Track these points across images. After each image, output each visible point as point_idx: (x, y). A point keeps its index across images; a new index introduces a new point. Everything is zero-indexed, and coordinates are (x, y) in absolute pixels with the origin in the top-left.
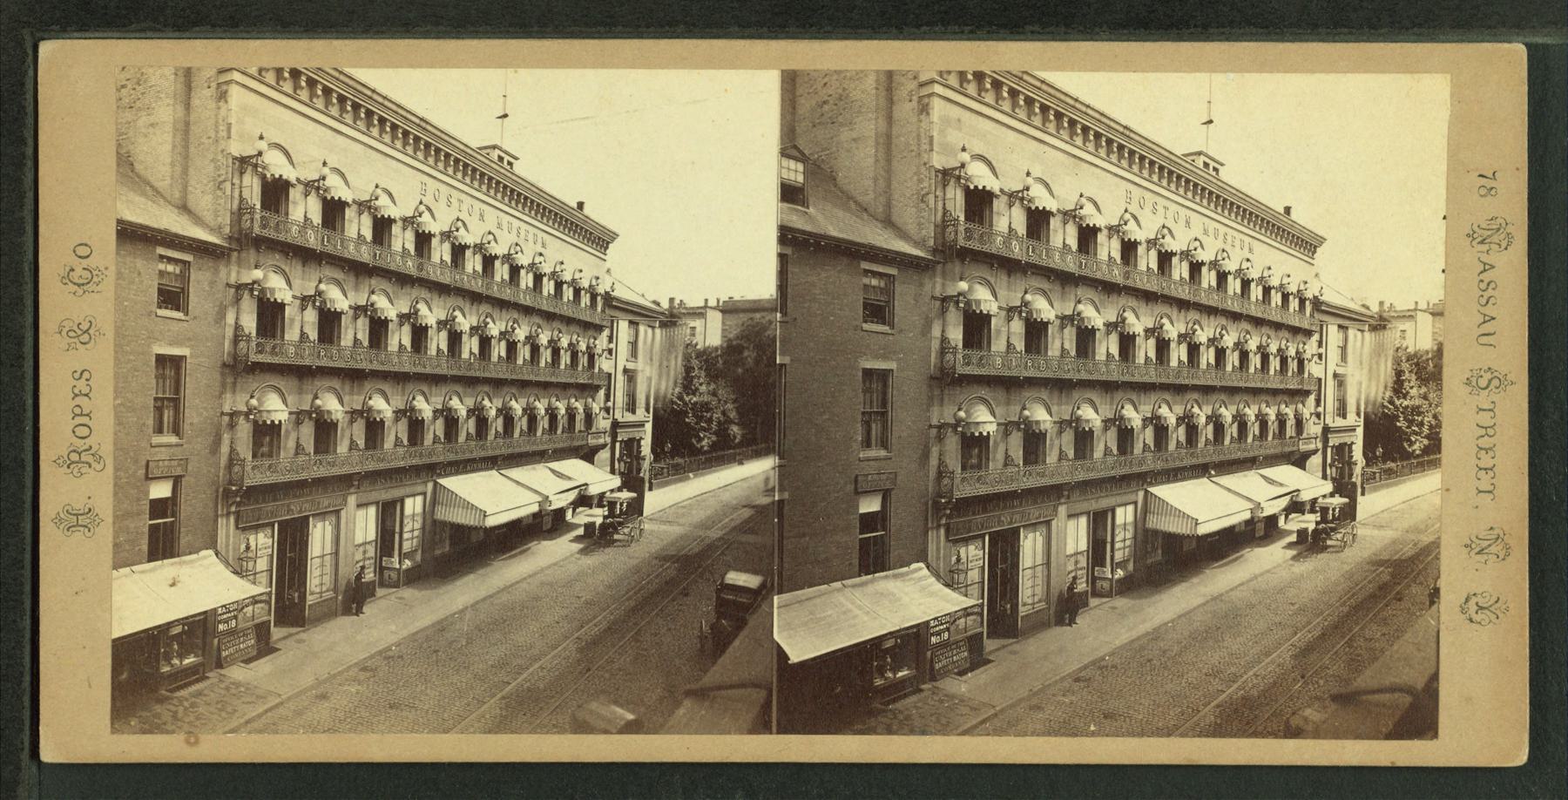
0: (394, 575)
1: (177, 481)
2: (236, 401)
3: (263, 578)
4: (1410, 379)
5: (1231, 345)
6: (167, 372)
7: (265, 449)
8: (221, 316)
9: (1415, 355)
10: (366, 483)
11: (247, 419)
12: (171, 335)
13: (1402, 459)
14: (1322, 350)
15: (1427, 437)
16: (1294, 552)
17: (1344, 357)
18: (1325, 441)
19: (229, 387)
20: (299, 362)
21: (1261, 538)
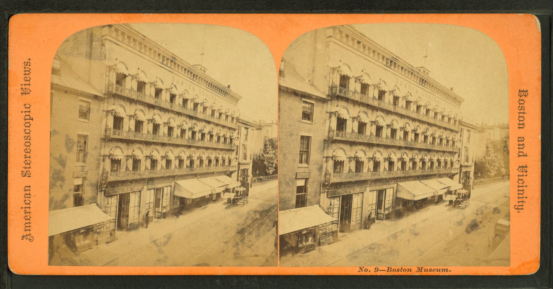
0: (382, 216)
1: (307, 180)
2: (106, 151)
3: (336, 215)
4: (269, 148)
5: (207, 132)
6: (305, 142)
7: (338, 170)
8: (101, 121)
9: (271, 139)
10: (373, 184)
11: (109, 158)
12: (306, 128)
13: (265, 175)
14: (239, 136)
15: (274, 168)
16: (226, 206)
17: (468, 141)
18: (239, 167)
19: (103, 146)
20: (351, 140)
21: (214, 201)
